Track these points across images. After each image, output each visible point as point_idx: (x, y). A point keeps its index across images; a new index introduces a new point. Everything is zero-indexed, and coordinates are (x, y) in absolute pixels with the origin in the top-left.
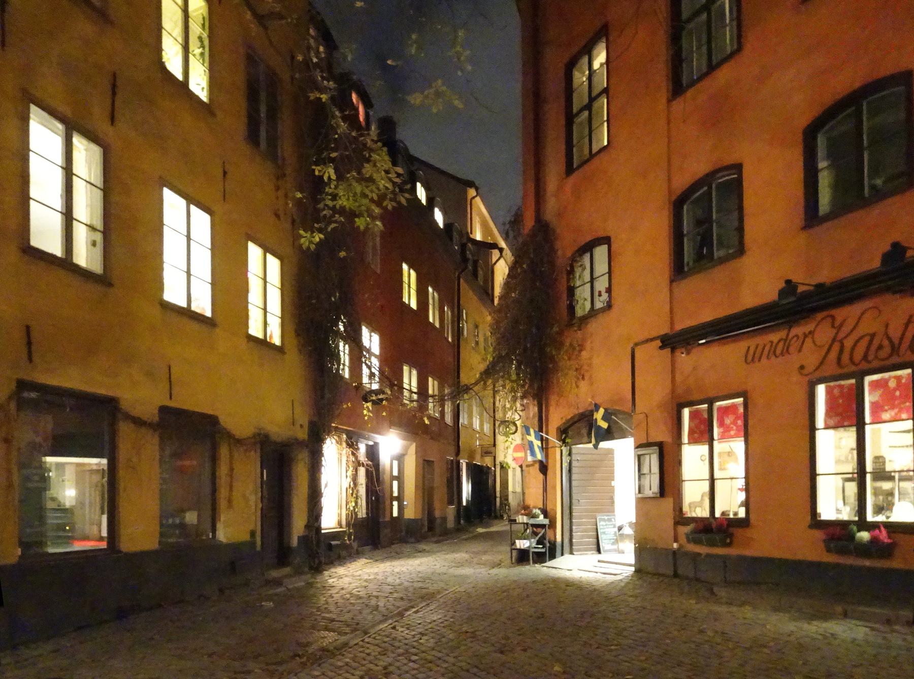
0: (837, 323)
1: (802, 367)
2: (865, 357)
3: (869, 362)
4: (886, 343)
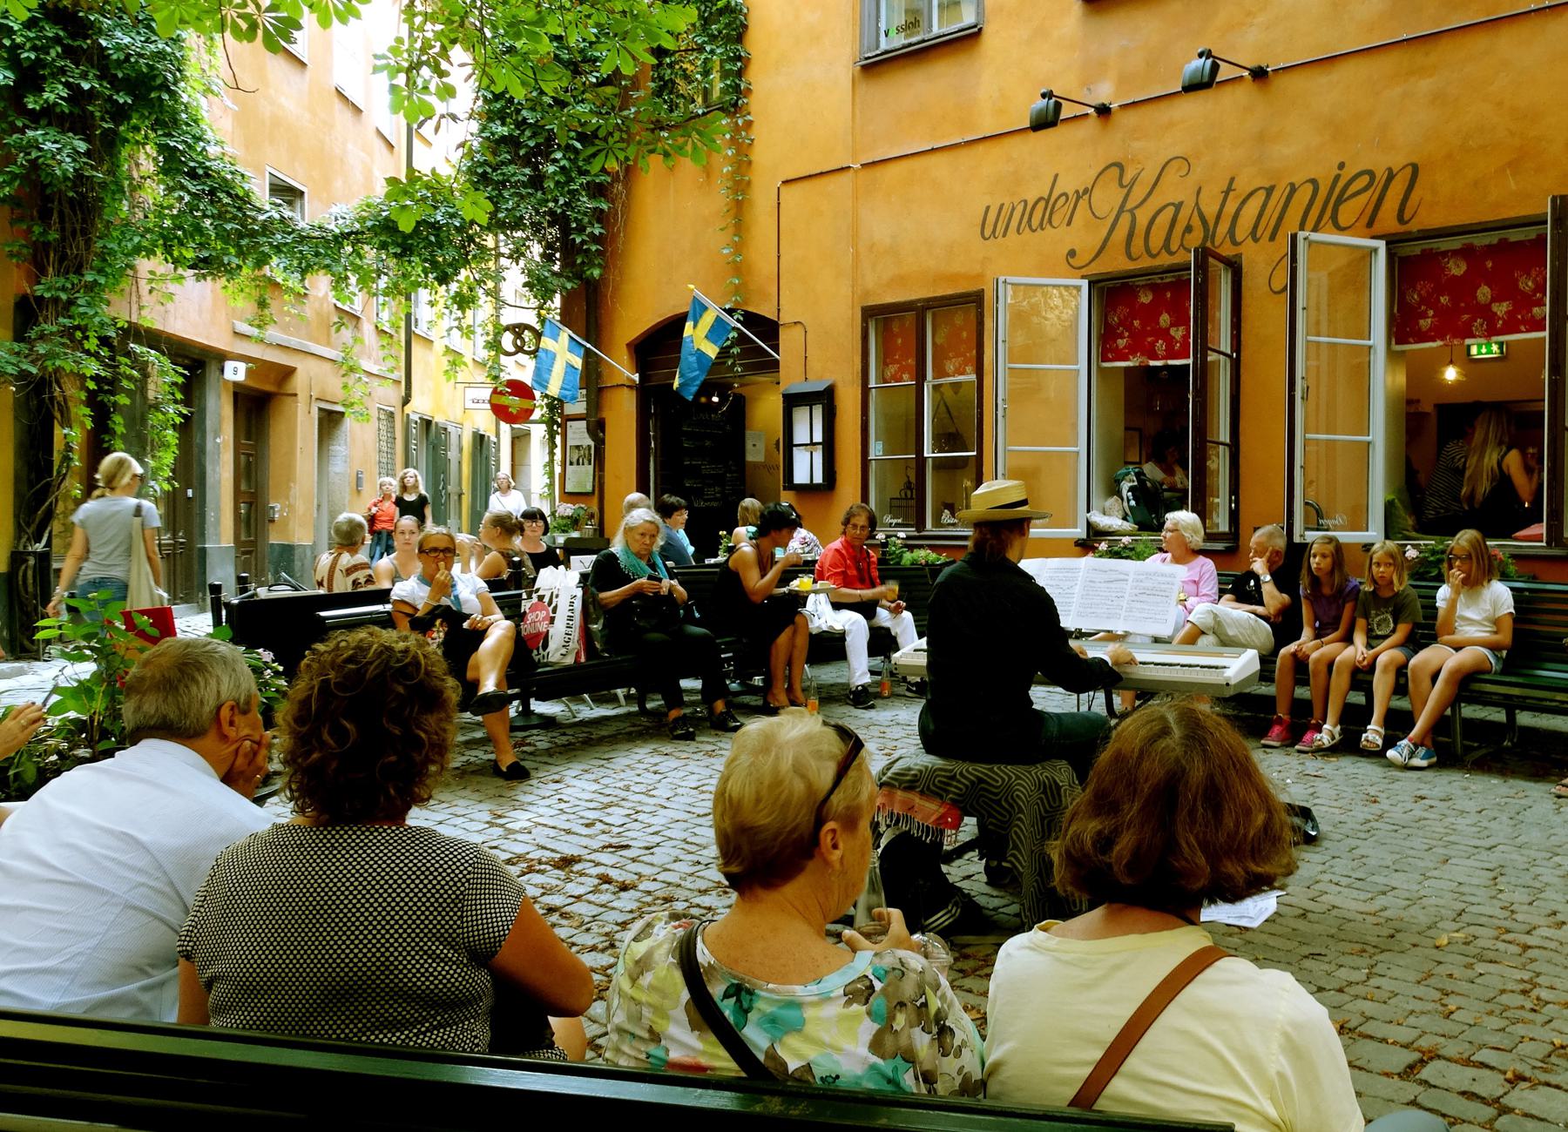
0: (1127, 179)
1: (1072, 253)
2: (1166, 245)
3: (1171, 253)
4: (1196, 222)
